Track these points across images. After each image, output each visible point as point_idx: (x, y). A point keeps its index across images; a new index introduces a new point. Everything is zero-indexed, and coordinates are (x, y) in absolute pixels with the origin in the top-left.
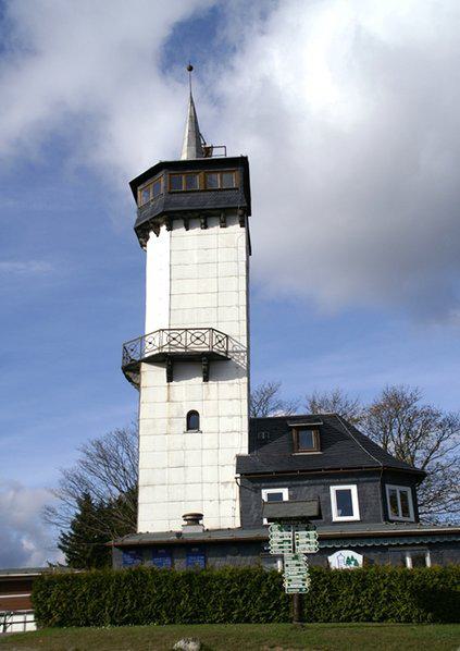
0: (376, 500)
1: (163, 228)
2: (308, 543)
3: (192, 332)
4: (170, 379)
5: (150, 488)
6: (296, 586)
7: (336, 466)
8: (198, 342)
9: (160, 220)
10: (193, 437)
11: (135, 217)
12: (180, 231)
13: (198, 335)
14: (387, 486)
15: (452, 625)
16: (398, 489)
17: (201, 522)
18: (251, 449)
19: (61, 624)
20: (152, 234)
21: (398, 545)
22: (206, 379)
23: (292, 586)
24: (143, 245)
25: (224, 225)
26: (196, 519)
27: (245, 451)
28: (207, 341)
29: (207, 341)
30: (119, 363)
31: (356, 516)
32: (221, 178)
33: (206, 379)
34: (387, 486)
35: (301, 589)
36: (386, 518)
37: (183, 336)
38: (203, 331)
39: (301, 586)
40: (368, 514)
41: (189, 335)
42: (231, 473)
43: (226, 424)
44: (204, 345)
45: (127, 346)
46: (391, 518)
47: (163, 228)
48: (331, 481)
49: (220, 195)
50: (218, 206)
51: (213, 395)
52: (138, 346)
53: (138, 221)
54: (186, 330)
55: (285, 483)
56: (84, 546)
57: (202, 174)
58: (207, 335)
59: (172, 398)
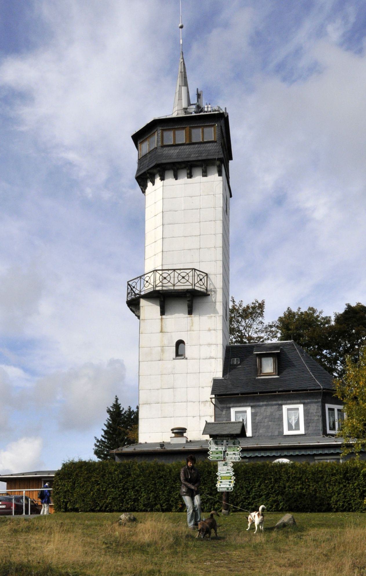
0: (317, 418)
1: (158, 180)
2: (234, 454)
3: (179, 271)
4: (163, 313)
5: (148, 406)
6: (224, 486)
7: (287, 389)
8: (183, 281)
9: (155, 171)
10: (180, 362)
11: (136, 167)
12: (170, 181)
13: (183, 274)
14: (328, 406)
15: (304, 514)
16: (336, 407)
17: (185, 434)
18: (225, 372)
19: (335, 512)
20: (150, 184)
21: (262, 457)
22: (190, 313)
23: (222, 486)
24: (144, 192)
25: (205, 174)
26: (180, 432)
27: (219, 375)
28: (190, 281)
29: (190, 281)
30: (123, 298)
31: (302, 431)
32: (203, 132)
33: (190, 313)
34: (328, 406)
35: (228, 488)
36: (325, 433)
37: (172, 275)
38: (188, 271)
39: (228, 486)
40: (311, 428)
41: (176, 275)
42: (207, 393)
43: (205, 352)
44: (188, 283)
45: (130, 283)
46: (329, 432)
47: (158, 180)
48: (283, 402)
49: (202, 148)
50: (200, 158)
51: (196, 327)
52: (138, 284)
53: (138, 170)
54: (174, 270)
55: (248, 404)
56: (136, 441)
57: (188, 129)
58: (191, 274)
59: (165, 330)
